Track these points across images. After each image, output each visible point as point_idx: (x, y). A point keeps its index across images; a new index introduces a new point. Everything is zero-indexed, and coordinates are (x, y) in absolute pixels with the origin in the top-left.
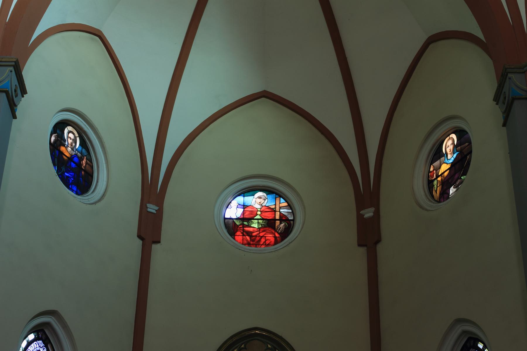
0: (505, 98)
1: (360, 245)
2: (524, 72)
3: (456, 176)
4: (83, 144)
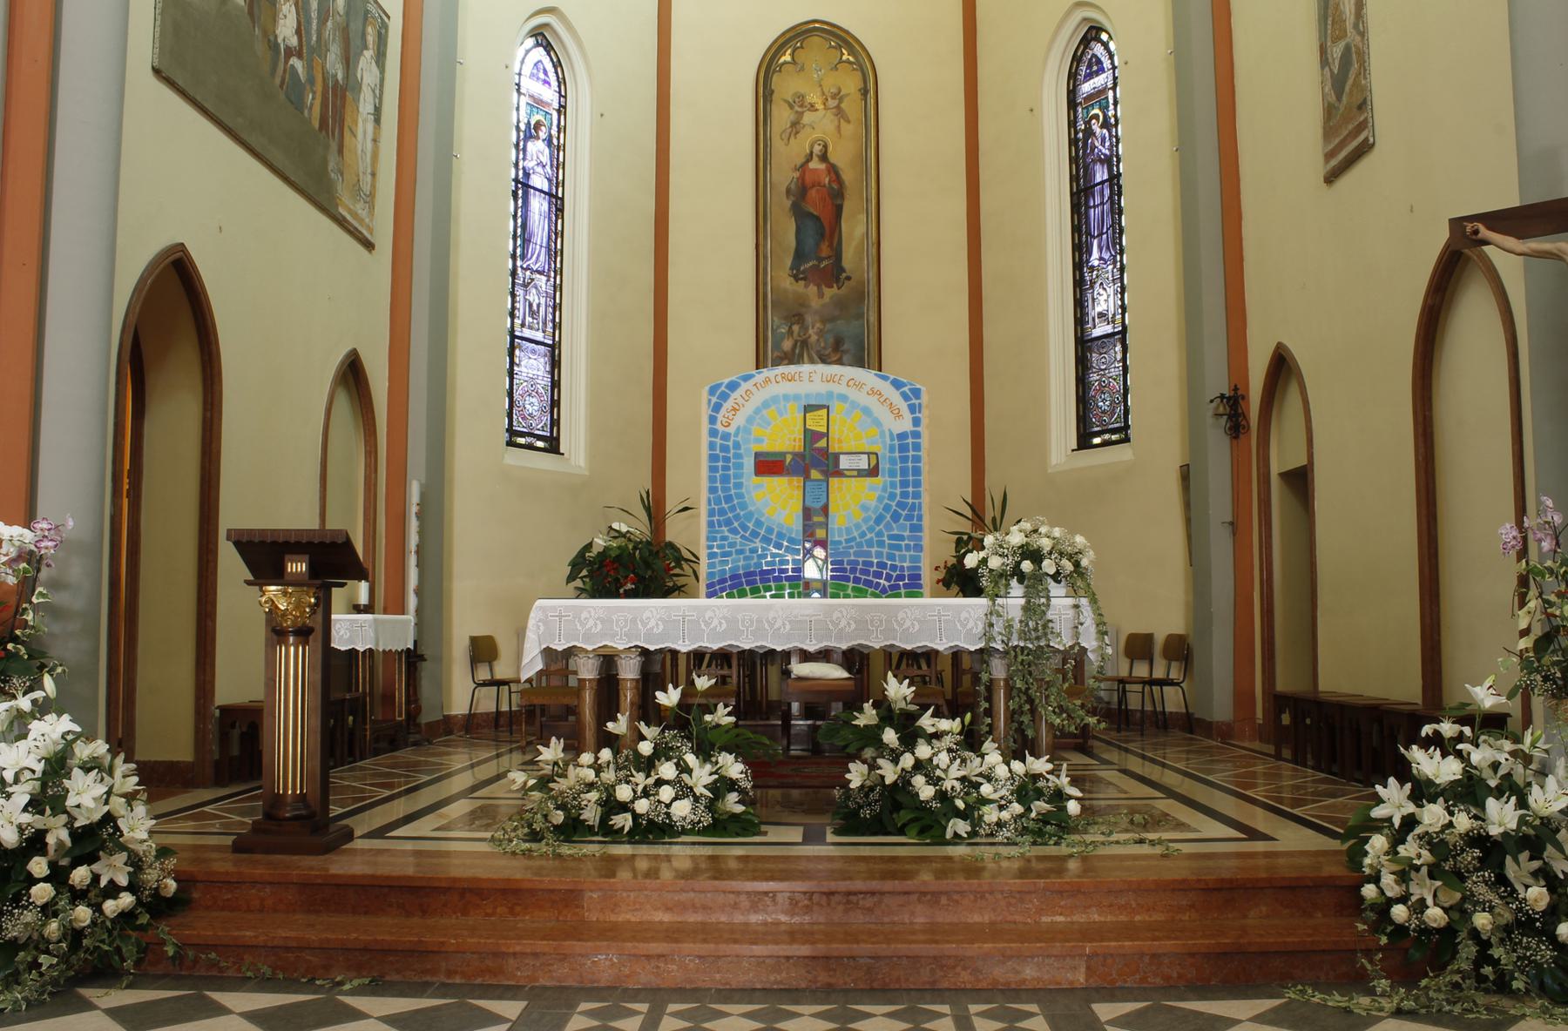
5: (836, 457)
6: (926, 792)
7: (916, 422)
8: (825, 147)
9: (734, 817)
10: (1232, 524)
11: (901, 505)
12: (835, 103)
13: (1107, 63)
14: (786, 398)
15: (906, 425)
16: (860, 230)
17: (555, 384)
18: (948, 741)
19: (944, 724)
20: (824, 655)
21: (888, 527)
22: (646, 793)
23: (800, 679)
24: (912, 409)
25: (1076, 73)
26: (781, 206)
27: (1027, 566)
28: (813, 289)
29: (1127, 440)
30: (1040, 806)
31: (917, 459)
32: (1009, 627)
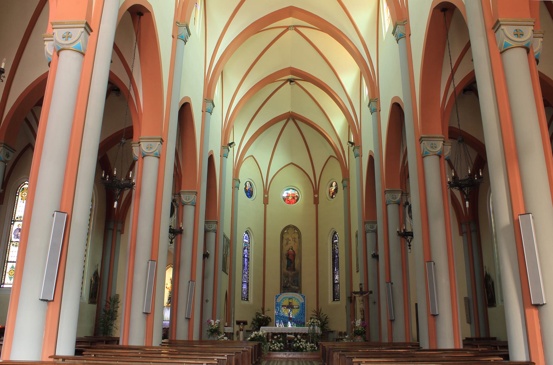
0: (396, 34)
1: (314, 204)
2: (404, 25)
3: (335, 193)
4: (251, 185)
5: (293, 306)
6: (301, 347)
7: (305, 301)
8: (292, 247)
9: (282, 350)
10: (350, 315)
11: (302, 313)
12: (294, 239)
13: (337, 238)
14: (286, 297)
15: (303, 302)
16: (298, 262)
17: (248, 289)
18: (304, 342)
19: (304, 340)
20: (291, 334)
21: (301, 316)
22: (273, 347)
23: (288, 337)
24: (304, 299)
25: (333, 238)
26: (285, 257)
27: (313, 324)
28: (290, 272)
29: (339, 300)
30: (313, 348)
31: (305, 306)
32: (311, 330)
